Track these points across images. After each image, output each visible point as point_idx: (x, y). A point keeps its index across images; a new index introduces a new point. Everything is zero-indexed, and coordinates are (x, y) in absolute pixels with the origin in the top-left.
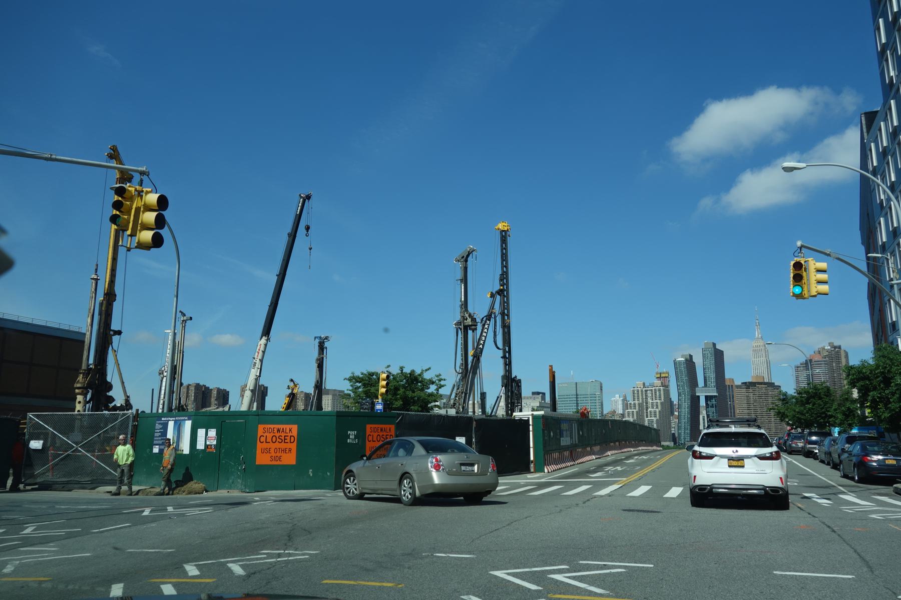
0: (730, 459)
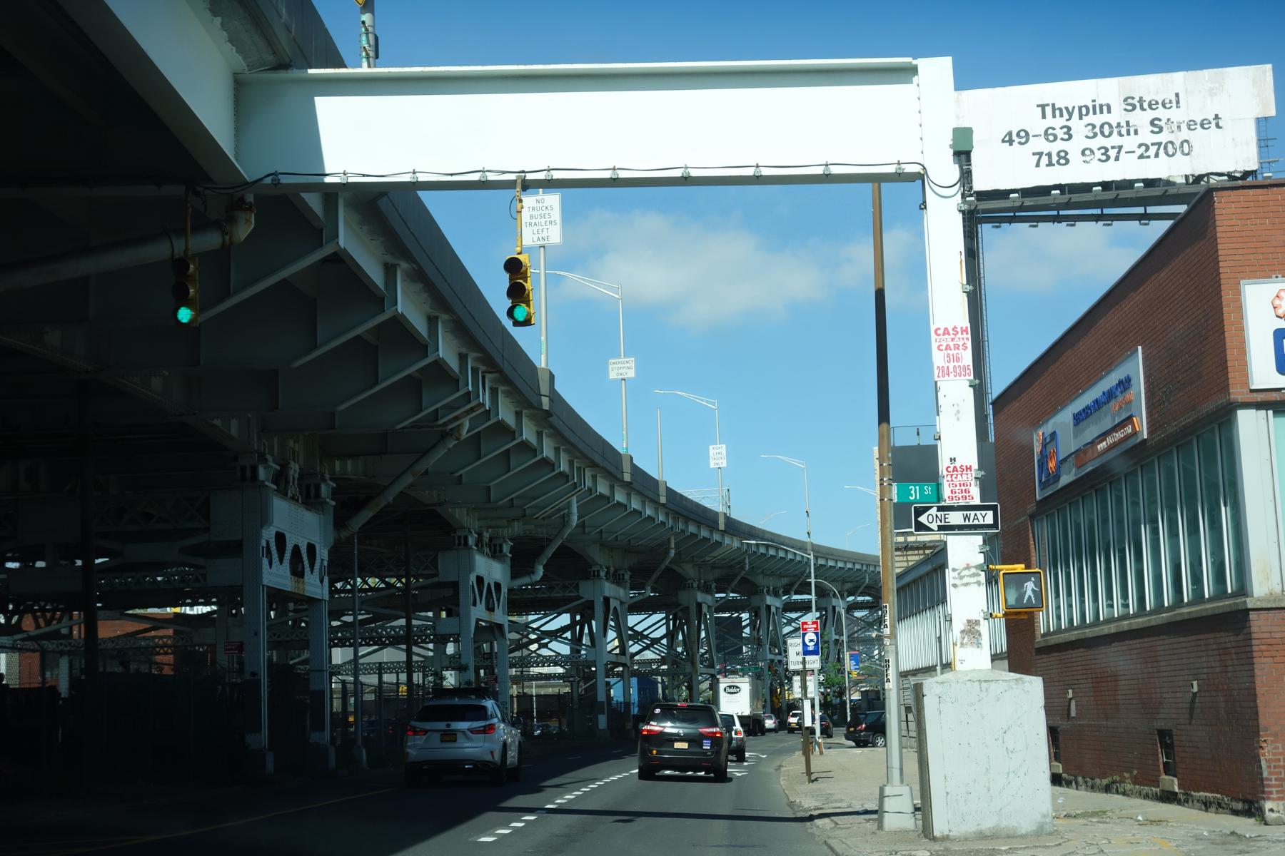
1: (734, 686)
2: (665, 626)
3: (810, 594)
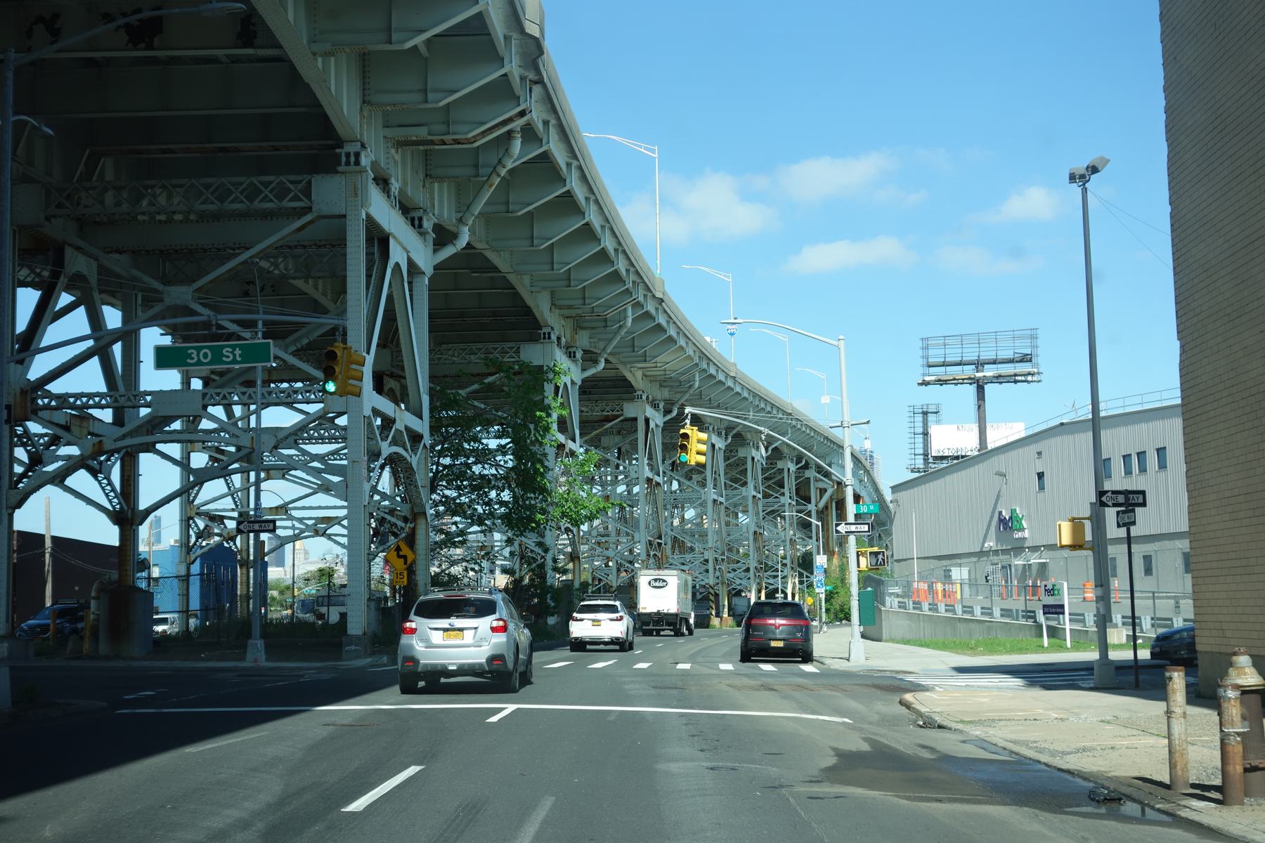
0: (445, 630)
1: (660, 579)
2: (143, 505)
3: (262, 192)
